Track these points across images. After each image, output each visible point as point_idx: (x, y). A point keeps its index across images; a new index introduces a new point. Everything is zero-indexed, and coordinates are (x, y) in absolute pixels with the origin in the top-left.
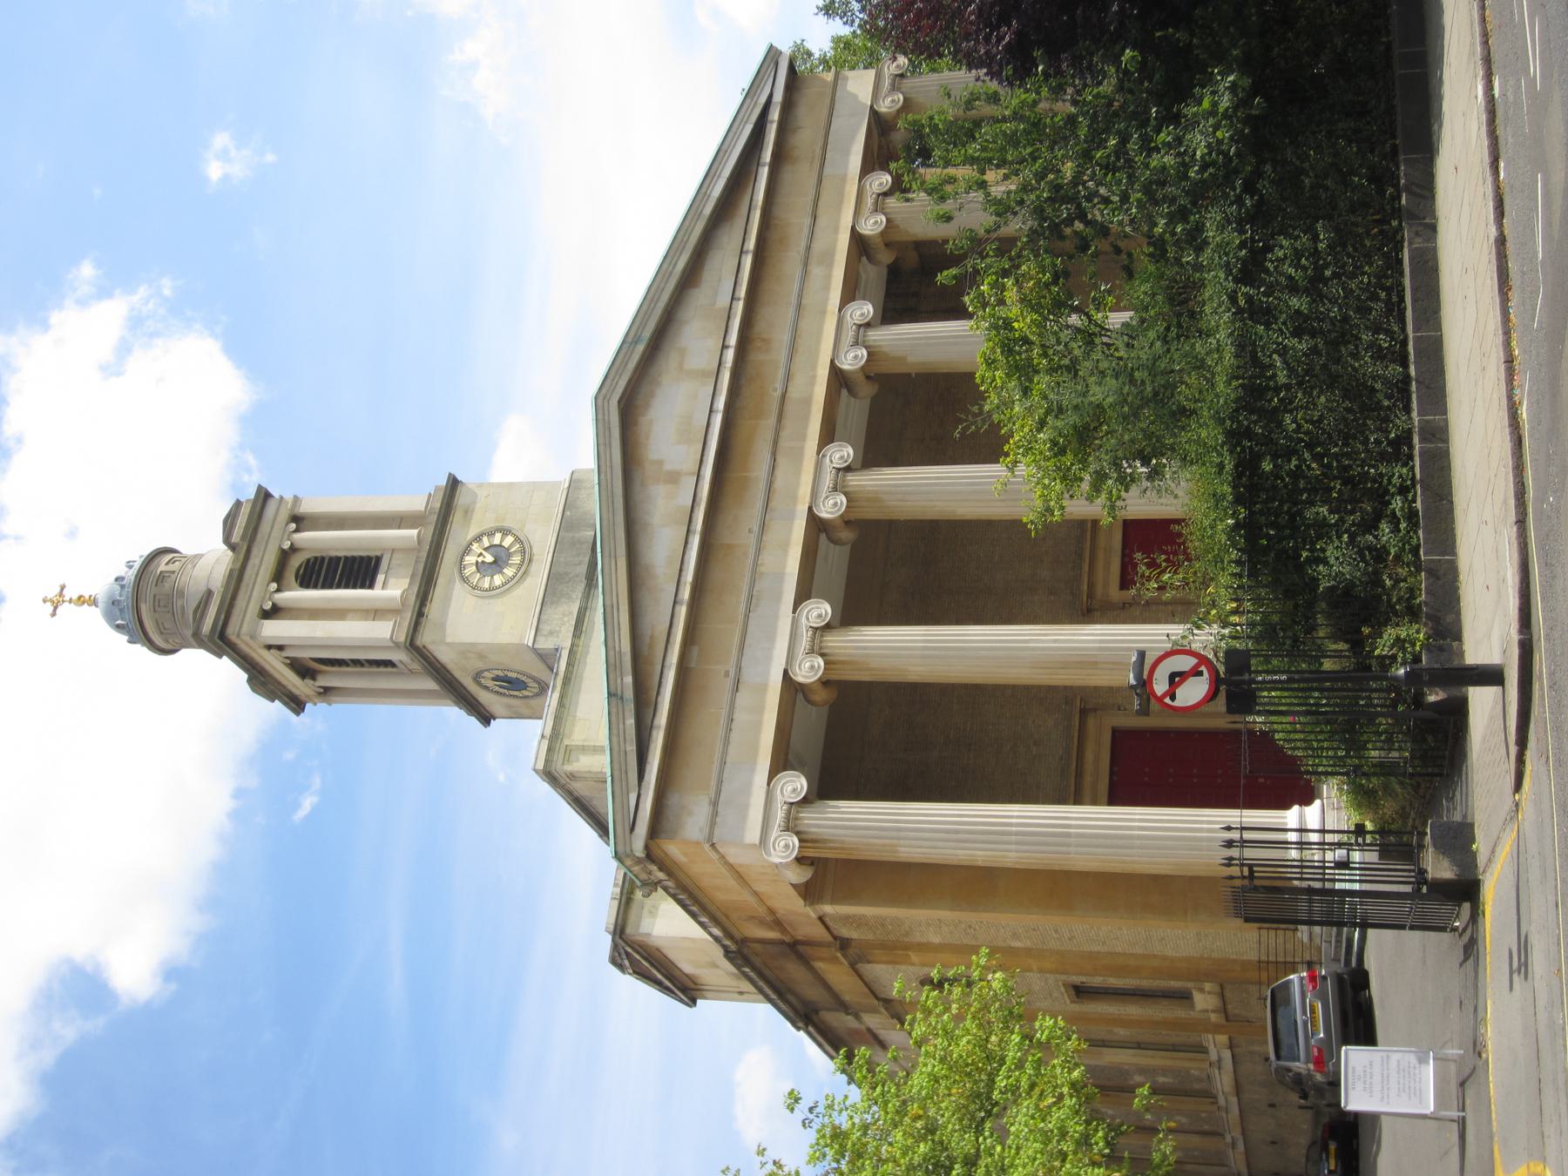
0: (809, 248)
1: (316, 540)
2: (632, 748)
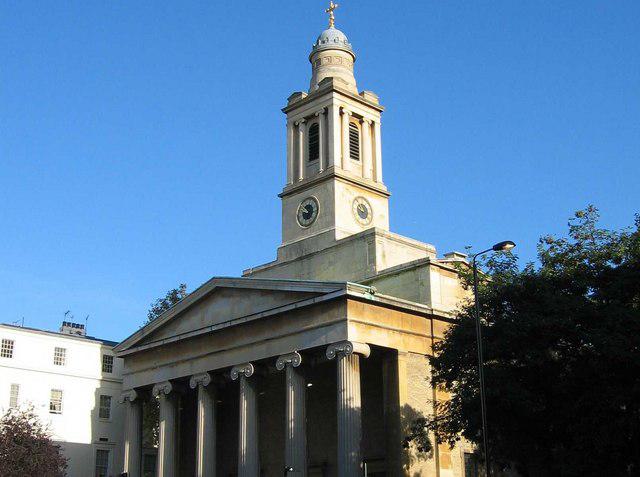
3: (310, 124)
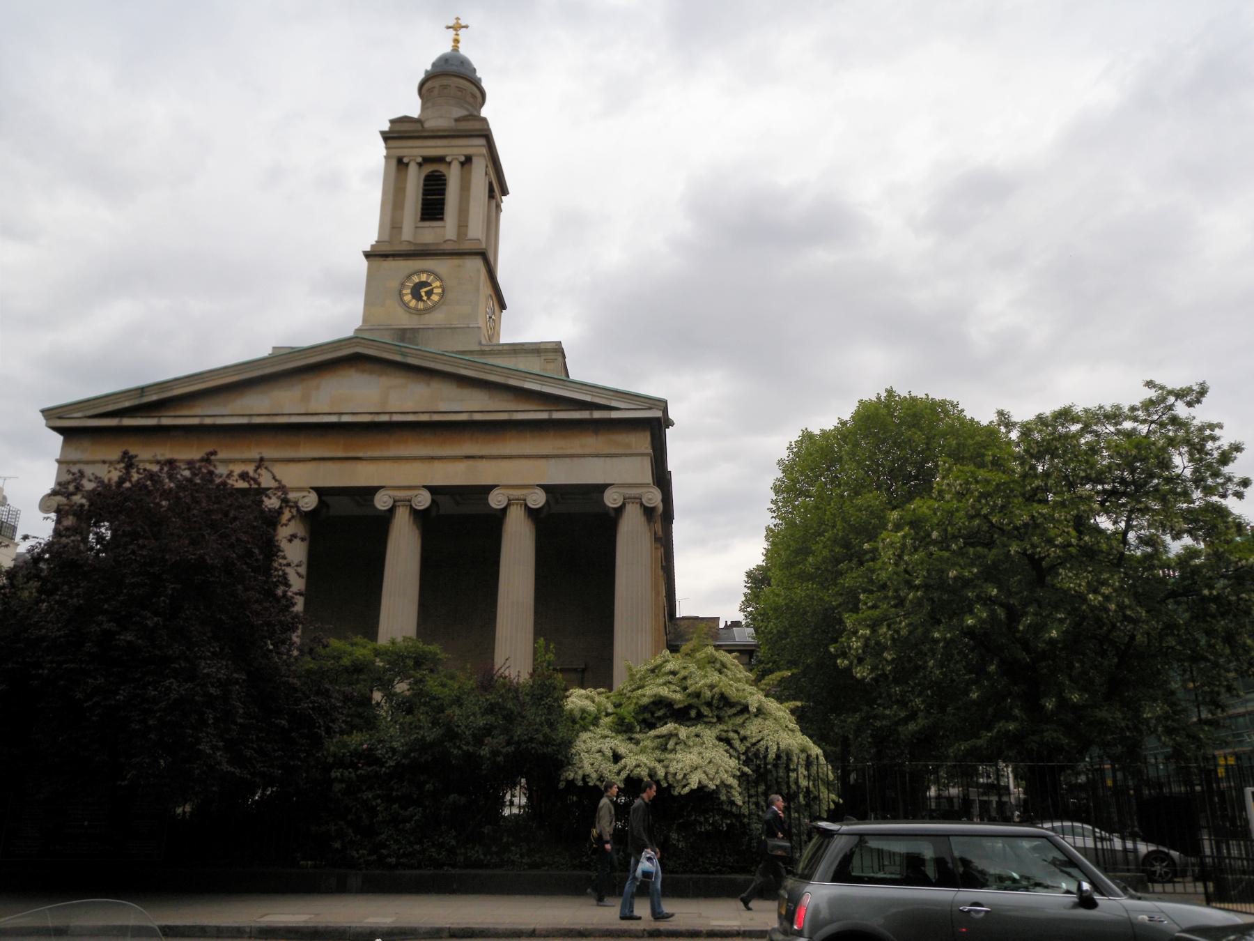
0: (482, 457)
1: (453, 176)
2: (110, 408)
3: (428, 169)
